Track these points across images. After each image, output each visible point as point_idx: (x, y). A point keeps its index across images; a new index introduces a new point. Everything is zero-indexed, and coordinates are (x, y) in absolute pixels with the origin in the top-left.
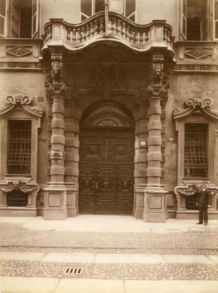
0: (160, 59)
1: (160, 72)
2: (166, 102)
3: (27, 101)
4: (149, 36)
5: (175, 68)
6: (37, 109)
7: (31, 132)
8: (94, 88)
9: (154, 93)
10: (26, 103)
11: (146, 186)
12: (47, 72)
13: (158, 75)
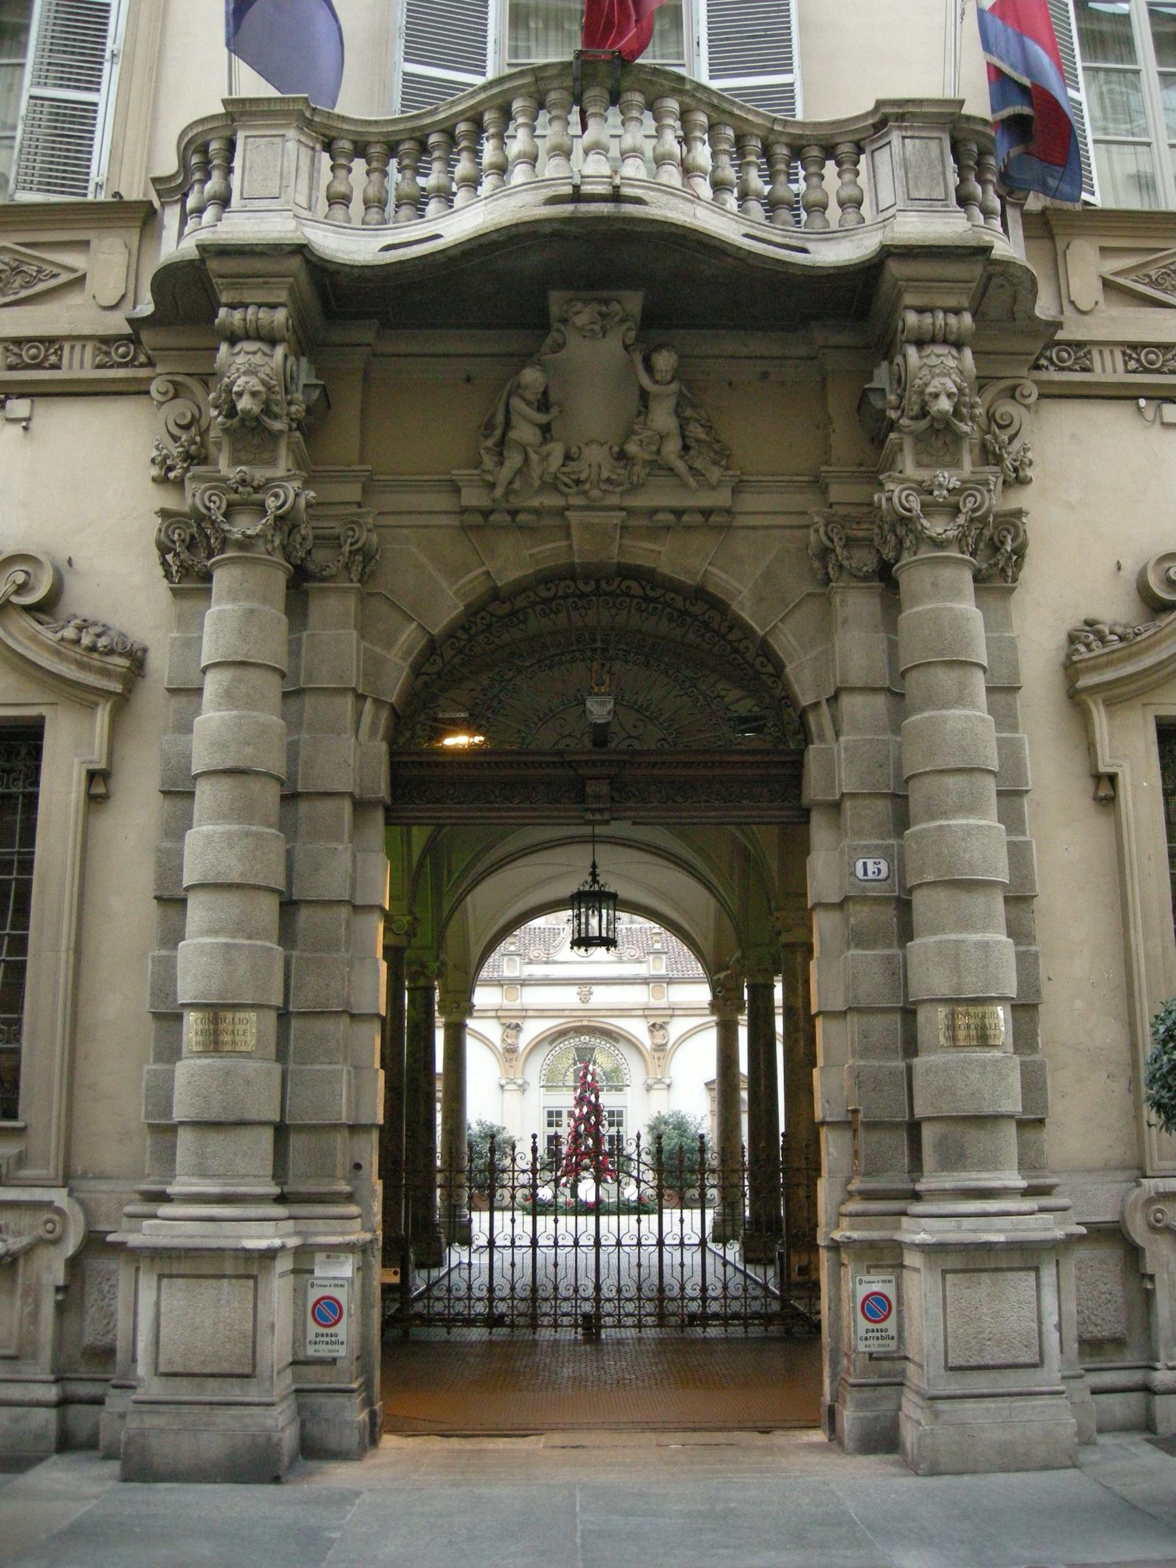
0: (952, 320)
1: (958, 398)
2: (1015, 580)
3: (22, 589)
4: (863, 180)
5: (1050, 360)
6: (86, 640)
7: (32, 801)
8: (499, 492)
9: (925, 522)
10: (15, 599)
11: (916, 1196)
12: (176, 396)
13: (943, 413)
